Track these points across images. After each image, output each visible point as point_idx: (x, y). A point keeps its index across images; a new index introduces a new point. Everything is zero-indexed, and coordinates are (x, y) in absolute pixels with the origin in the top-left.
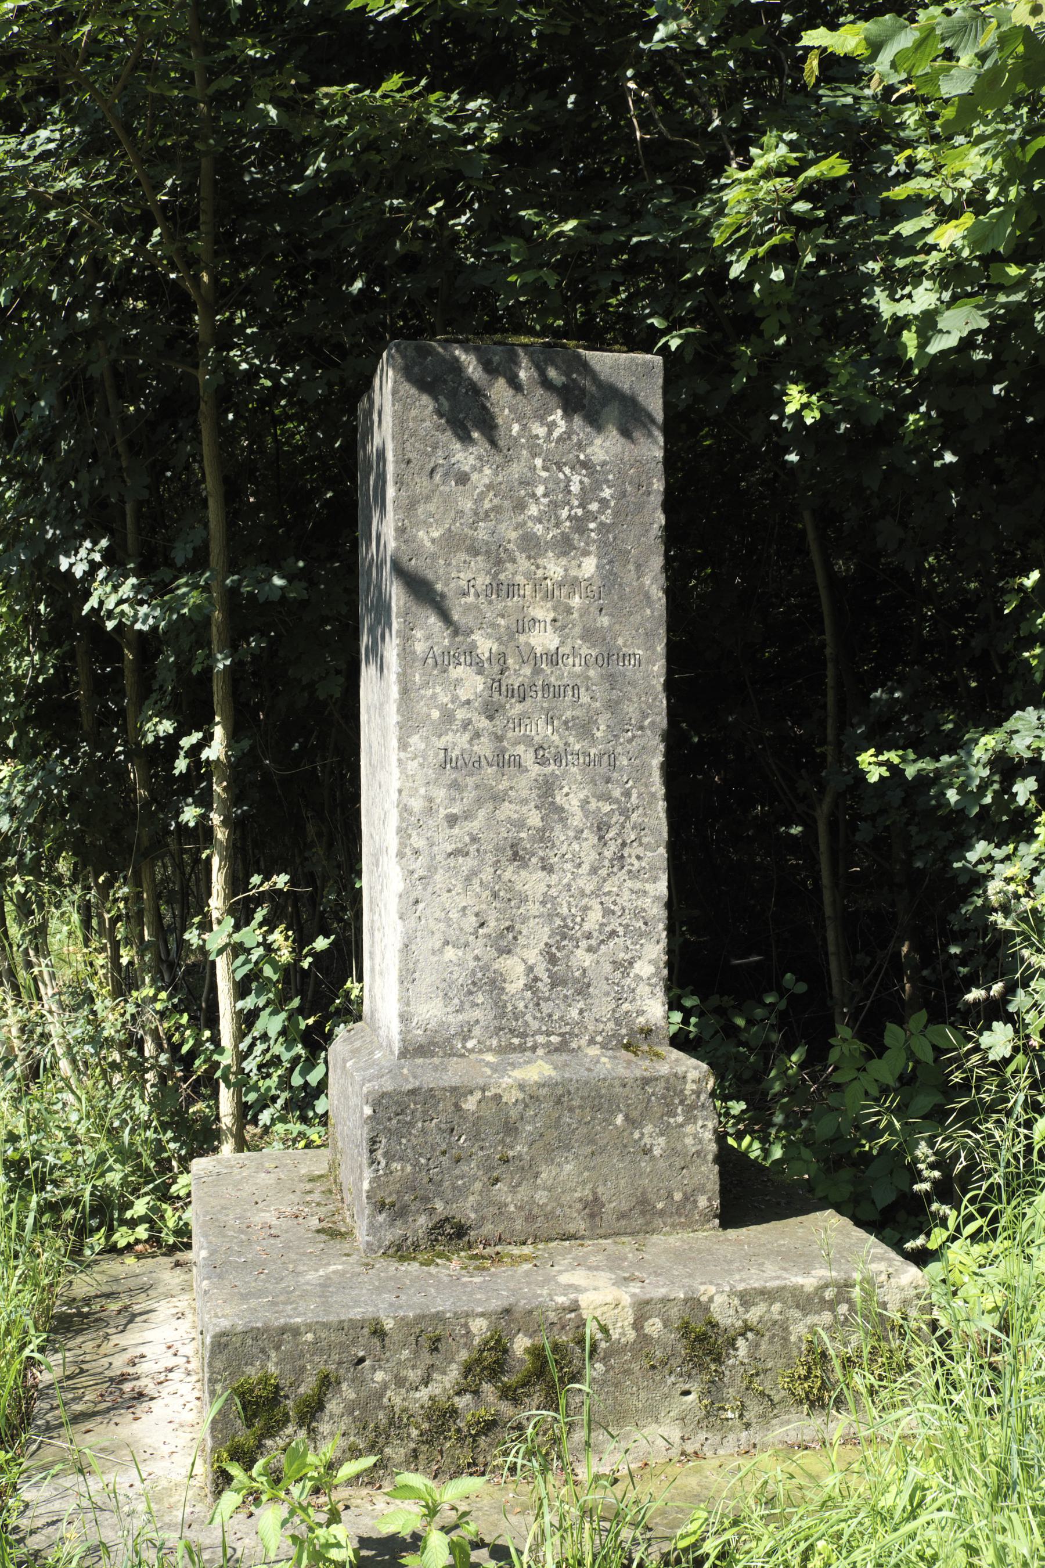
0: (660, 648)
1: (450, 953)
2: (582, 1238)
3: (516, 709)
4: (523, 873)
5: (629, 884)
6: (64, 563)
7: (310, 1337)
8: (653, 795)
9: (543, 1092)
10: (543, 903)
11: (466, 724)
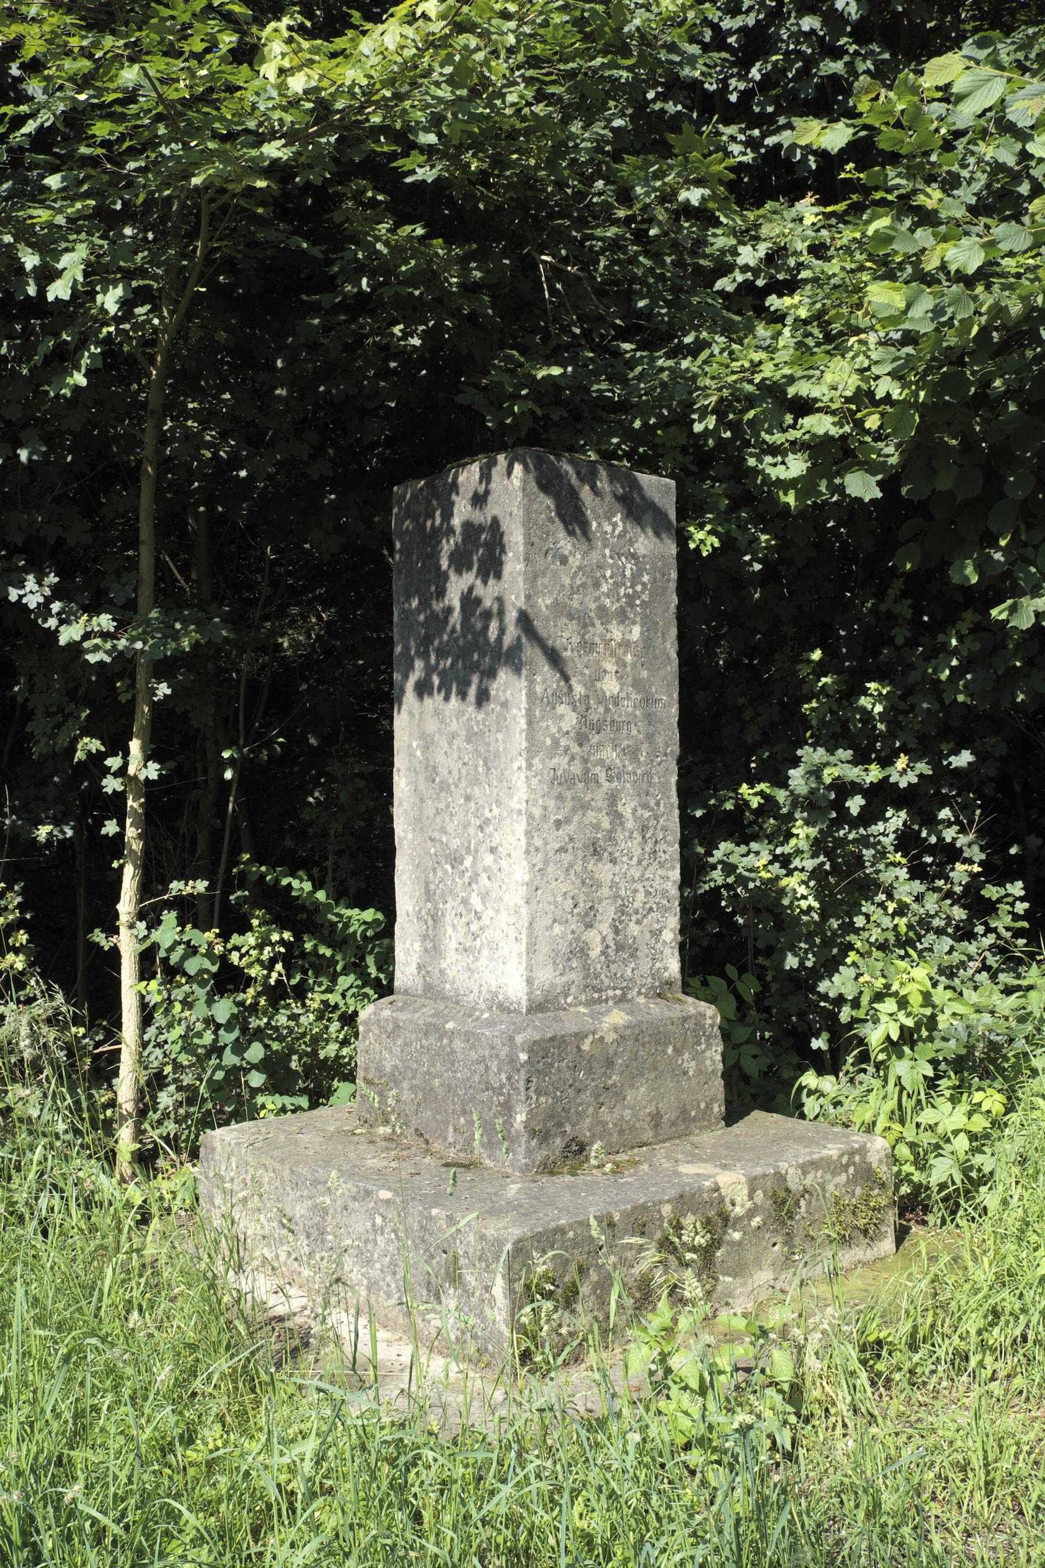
0: (676, 695)
1: (558, 929)
2: (650, 1144)
3: (595, 739)
4: (600, 865)
5: (659, 872)
6: (13, 594)
7: (571, 1234)
8: (672, 805)
9: (628, 1032)
10: (611, 887)
11: (567, 749)
